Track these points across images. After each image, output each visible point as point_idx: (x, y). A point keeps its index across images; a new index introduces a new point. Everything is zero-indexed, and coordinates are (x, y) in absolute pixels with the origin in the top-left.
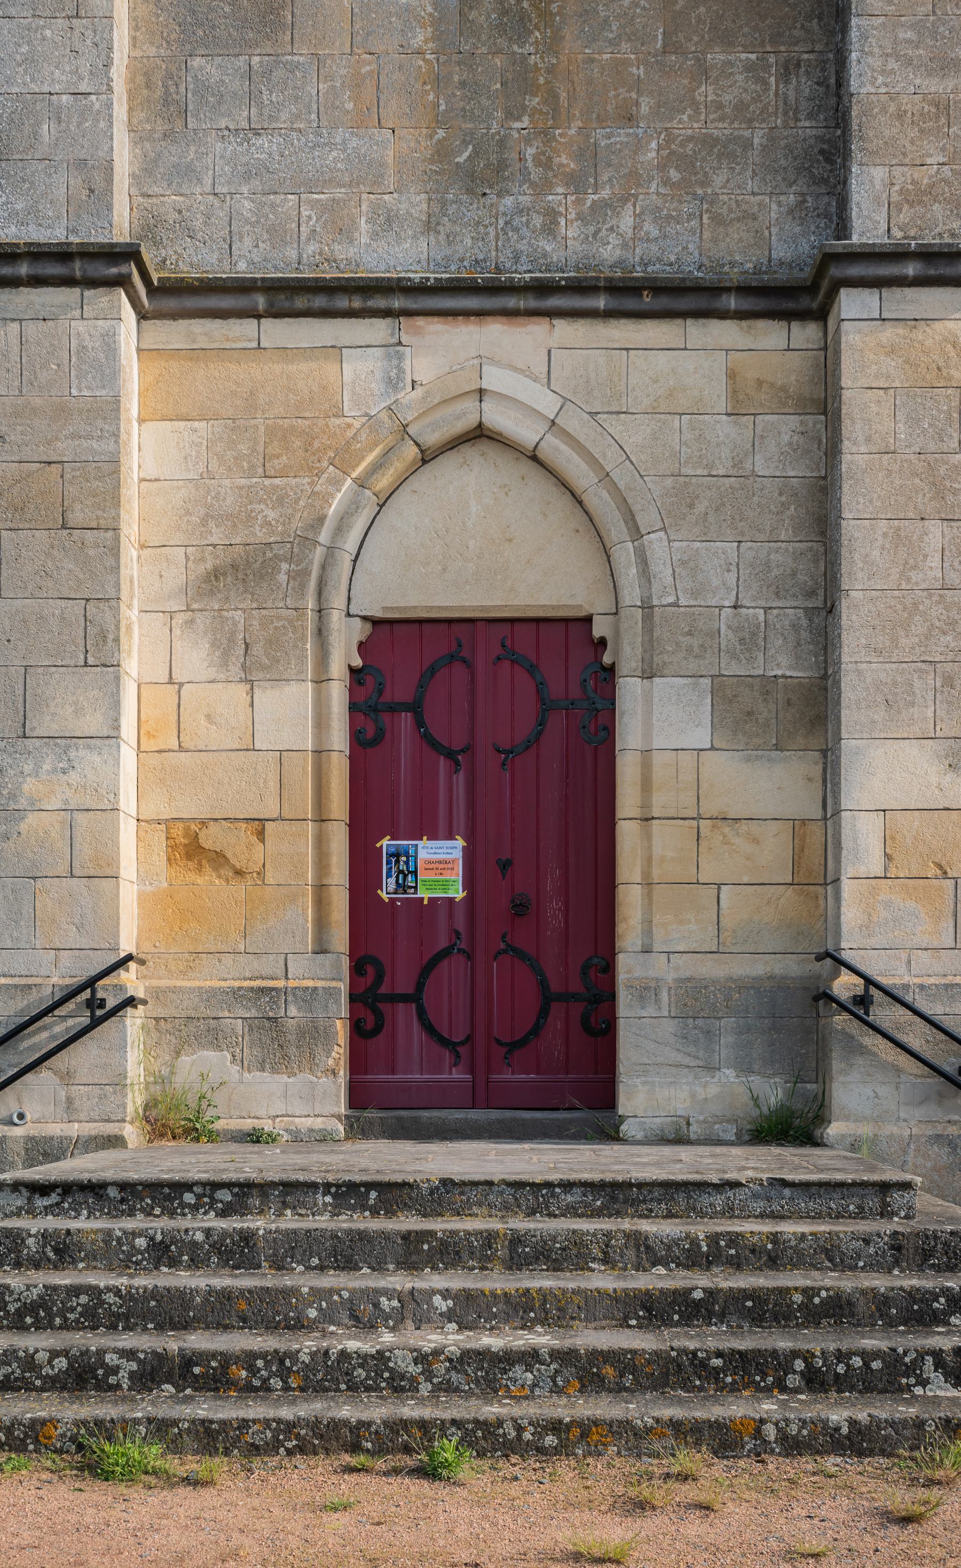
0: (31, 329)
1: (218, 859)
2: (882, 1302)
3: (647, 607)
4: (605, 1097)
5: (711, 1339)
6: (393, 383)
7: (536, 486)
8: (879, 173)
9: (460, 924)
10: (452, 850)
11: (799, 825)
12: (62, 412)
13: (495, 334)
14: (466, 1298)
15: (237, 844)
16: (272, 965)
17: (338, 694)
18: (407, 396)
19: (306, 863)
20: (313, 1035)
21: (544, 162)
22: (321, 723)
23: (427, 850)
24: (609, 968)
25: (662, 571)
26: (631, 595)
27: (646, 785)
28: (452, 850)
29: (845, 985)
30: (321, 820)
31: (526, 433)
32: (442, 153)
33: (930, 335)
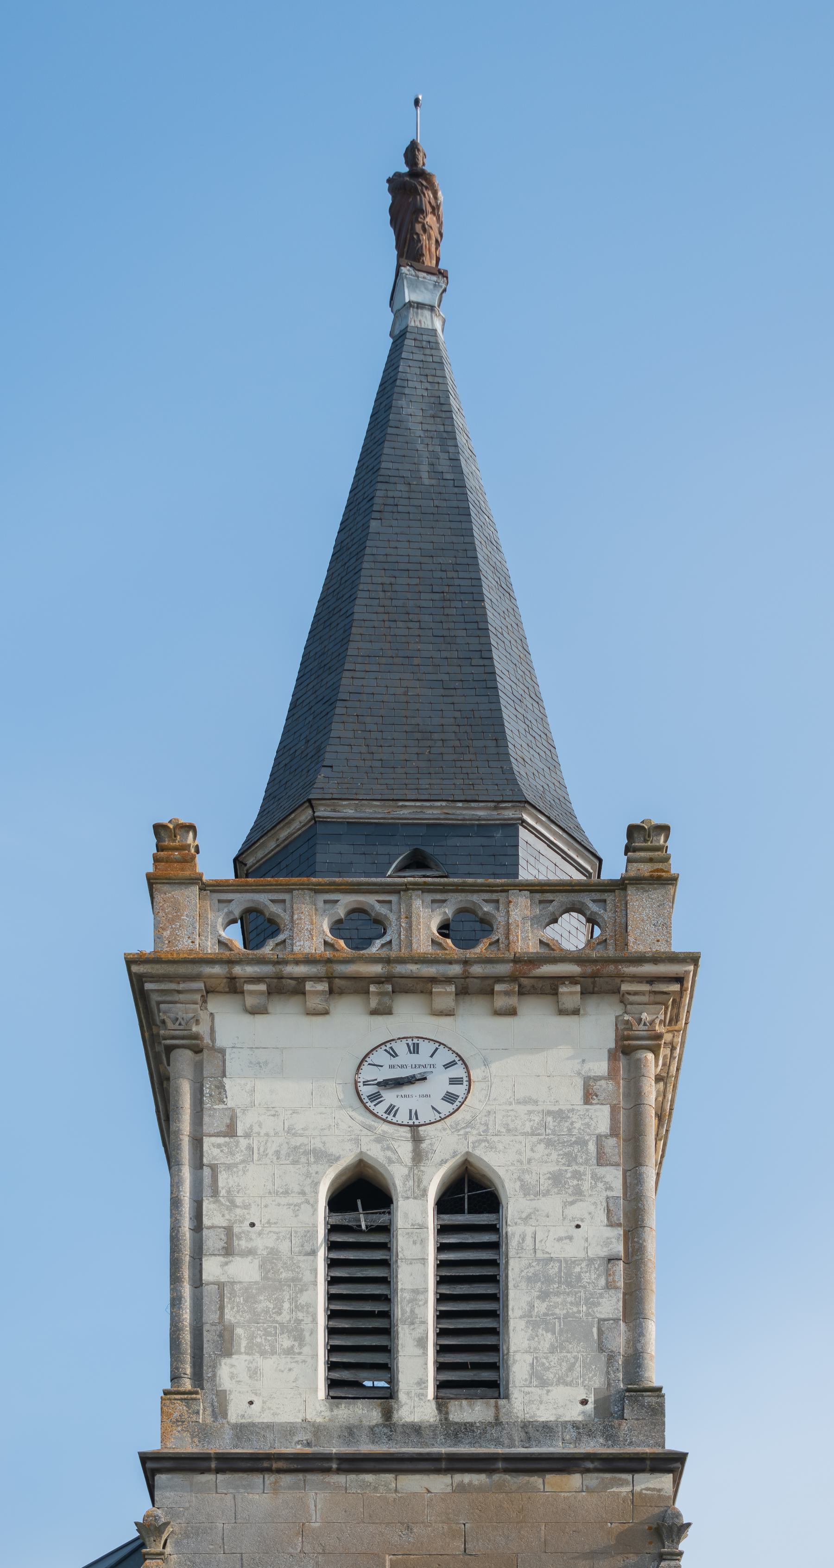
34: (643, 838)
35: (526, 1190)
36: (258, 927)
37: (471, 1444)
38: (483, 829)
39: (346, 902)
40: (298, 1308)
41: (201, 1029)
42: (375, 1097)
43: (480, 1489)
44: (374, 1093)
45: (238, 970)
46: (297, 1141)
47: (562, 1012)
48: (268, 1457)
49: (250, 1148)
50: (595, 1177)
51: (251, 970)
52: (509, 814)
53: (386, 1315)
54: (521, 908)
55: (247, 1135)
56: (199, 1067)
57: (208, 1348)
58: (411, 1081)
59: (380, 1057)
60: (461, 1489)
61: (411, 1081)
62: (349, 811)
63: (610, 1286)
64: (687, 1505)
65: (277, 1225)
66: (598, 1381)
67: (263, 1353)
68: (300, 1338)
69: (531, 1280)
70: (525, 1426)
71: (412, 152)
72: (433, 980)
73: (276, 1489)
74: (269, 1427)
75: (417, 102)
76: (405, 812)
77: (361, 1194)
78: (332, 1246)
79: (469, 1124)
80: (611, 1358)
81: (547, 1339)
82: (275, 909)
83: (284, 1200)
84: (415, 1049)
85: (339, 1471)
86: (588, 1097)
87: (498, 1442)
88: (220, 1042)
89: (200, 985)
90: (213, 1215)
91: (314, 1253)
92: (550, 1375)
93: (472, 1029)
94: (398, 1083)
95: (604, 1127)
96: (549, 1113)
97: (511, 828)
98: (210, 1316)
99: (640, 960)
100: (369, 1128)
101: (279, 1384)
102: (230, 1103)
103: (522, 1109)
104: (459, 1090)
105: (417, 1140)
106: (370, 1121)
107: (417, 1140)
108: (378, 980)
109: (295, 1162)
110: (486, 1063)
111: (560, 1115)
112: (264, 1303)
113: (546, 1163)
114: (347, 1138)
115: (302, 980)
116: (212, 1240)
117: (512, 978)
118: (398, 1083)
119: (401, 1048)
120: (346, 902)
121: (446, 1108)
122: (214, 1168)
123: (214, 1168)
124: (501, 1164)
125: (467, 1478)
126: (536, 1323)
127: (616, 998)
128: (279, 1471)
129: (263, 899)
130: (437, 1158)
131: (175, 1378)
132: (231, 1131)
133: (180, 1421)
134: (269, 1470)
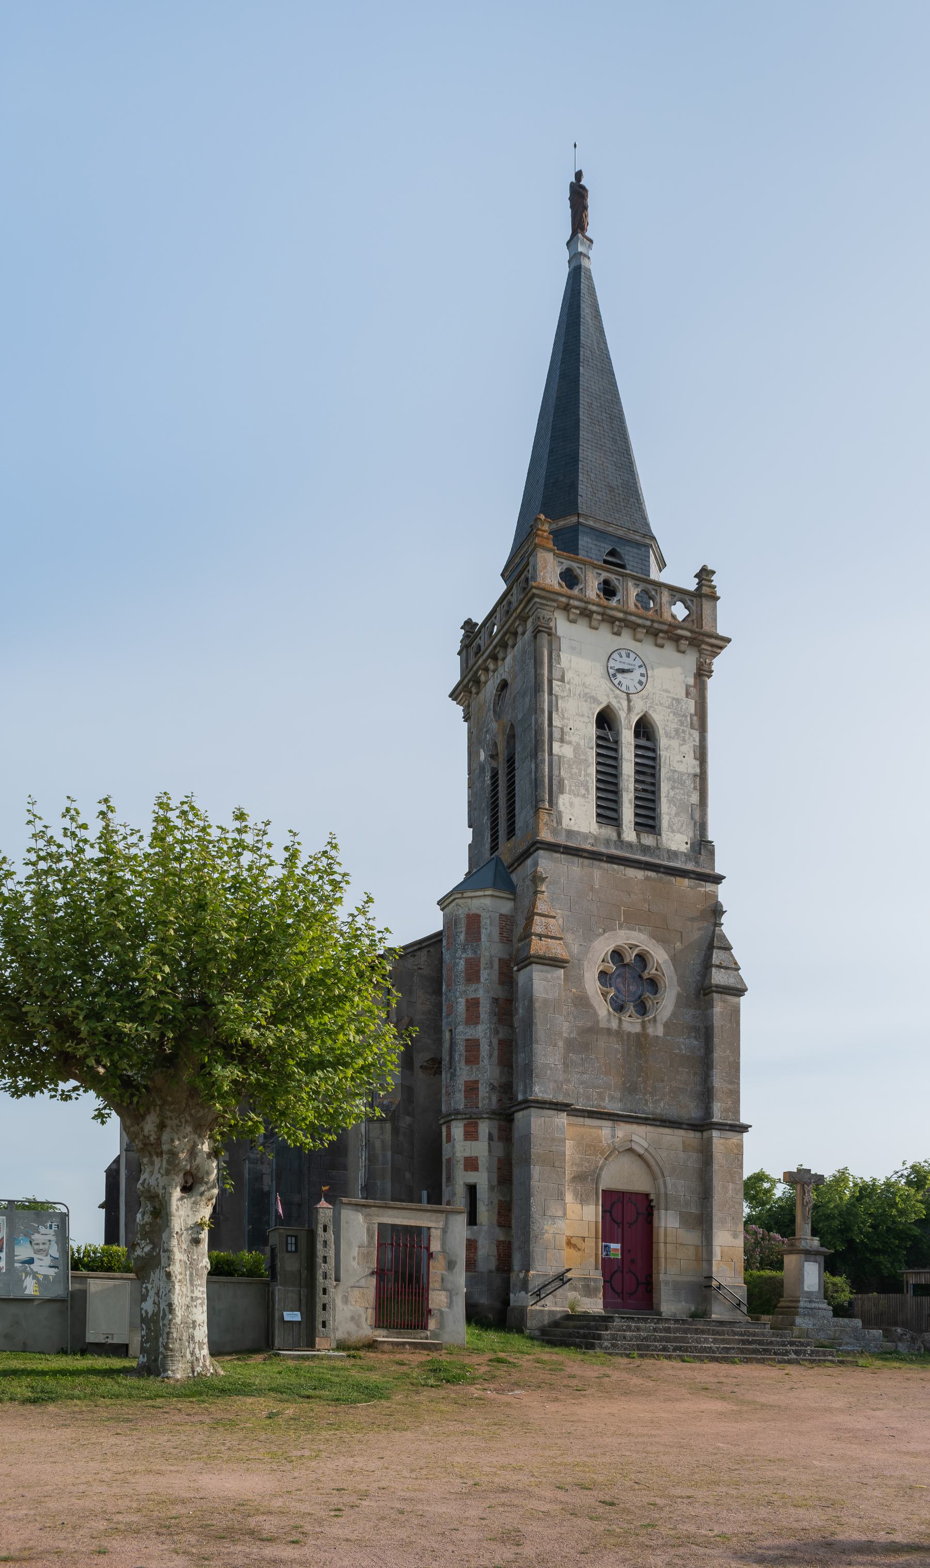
0: (547, 1119)
1: (575, 1246)
2: (778, 1342)
6: (613, 1136)
7: (640, 1162)
9: (620, 1265)
10: (618, 1246)
12: (553, 1140)
13: (634, 1127)
14: (714, 1339)
18: (617, 1140)
20: (596, 1289)
21: (645, 1089)
22: (597, 1215)
25: (669, 1186)
26: (662, 1191)
27: (666, 1235)
28: (618, 1246)
30: (597, 1238)
31: (641, 1151)
32: (624, 1083)
34: (704, 575)
35: (668, 736)
37: (650, 857)
41: (552, 624)
42: (614, 675)
43: (654, 880)
44: (615, 674)
45: (572, 602)
46: (587, 691)
49: (570, 690)
50: (691, 735)
51: (576, 603)
55: (569, 683)
59: (615, 656)
63: (695, 788)
66: (691, 834)
67: (574, 795)
69: (669, 779)
70: (669, 851)
71: (579, 175)
72: (639, 625)
74: (578, 833)
75: (575, 146)
80: (695, 823)
82: (579, 571)
83: (582, 719)
85: (607, 862)
86: (688, 694)
87: (659, 858)
89: (555, 604)
90: (556, 722)
94: (623, 671)
95: (692, 711)
96: (674, 699)
98: (555, 772)
100: (612, 690)
102: (562, 666)
103: (665, 694)
104: (644, 679)
105: (629, 700)
106: (613, 687)
107: (629, 700)
108: (620, 620)
109: (586, 701)
110: (653, 669)
111: (678, 701)
112: (575, 770)
115: (592, 612)
116: (556, 734)
117: (666, 632)
118: (623, 671)
119: (623, 653)
121: (639, 687)
123: (557, 696)
125: (650, 873)
126: (671, 801)
127: (696, 649)
128: (585, 857)
132: (562, 680)
134: (581, 856)
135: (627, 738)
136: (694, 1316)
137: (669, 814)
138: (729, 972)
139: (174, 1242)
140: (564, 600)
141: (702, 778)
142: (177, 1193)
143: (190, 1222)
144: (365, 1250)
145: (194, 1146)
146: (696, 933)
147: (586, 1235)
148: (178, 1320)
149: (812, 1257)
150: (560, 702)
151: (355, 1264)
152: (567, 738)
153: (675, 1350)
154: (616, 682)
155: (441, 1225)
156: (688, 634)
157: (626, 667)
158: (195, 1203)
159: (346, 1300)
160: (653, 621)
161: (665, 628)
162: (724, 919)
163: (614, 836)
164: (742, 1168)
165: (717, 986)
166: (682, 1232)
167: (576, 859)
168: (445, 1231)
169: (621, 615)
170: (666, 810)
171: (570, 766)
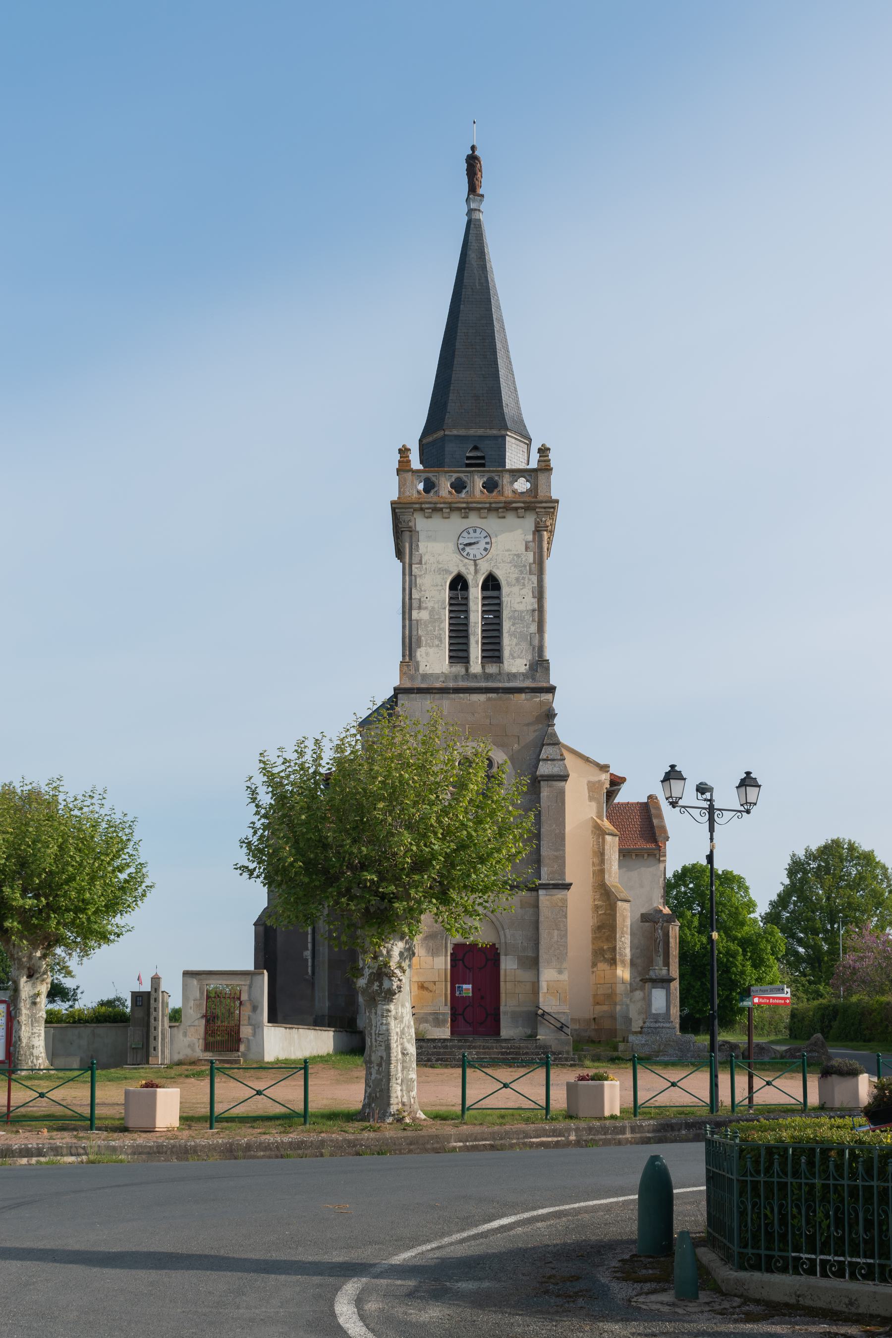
1: (427, 989)
3: (506, 943)
4: (498, 1033)
5: (407, 640)
8: (546, 869)
10: (470, 986)
11: (533, 983)
15: (431, 986)
16: (437, 1008)
17: (449, 958)
19: (443, 989)
20: (444, 1022)
23: (465, 986)
24: (499, 1009)
26: (503, 941)
27: (506, 976)
28: (470, 986)
29: (540, 1012)
30: (446, 981)
33: (555, 898)
35: (509, 584)
36: (429, 486)
38: (496, 438)
39: (455, 475)
40: (440, 629)
42: (463, 549)
43: (495, 699)
44: (463, 549)
46: (440, 566)
47: (519, 517)
48: (432, 689)
50: (529, 579)
51: (427, 506)
52: (503, 432)
53: (467, 631)
54: (507, 478)
56: (411, 537)
57: (413, 645)
58: (474, 543)
59: (465, 534)
60: (489, 699)
61: (474, 543)
62: (455, 432)
63: (533, 621)
64: (557, 706)
65: (436, 595)
66: (530, 657)
68: (441, 641)
69: (510, 618)
71: (473, 148)
72: (481, 508)
73: (434, 699)
74: (431, 675)
76: (472, 432)
77: (459, 584)
78: (450, 605)
79: (491, 559)
80: (534, 648)
81: (515, 641)
84: (475, 531)
86: (527, 549)
87: (500, 681)
88: (418, 529)
91: (445, 608)
92: (515, 655)
93: (492, 523)
95: (531, 561)
97: (503, 437)
98: (414, 633)
99: (541, 502)
101: (435, 660)
103: (507, 553)
104: (488, 546)
105: (476, 565)
107: (476, 565)
108: (464, 508)
111: (518, 556)
113: (514, 574)
114: (455, 564)
116: (415, 604)
119: (471, 531)
120: (455, 475)
121: (484, 553)
122: (415, 576)
123: (415, 576)
124: (500, 574)
125: (491, 695)
129: (430, 475)
130: (482, 572)
131: (404, 656)
132: (420, 563)
133: (405, 673)
135: (476, 594)
136: (530, 1036)
137: (510, 645)
138: (555, 762)
139: (22, 1004)
140: (417, 506)
141: (540, 610)
142: (24, 979)
143: (31, 994)
144: (198, 1002)
145: (31, 954)
146: (531, 735)
147: (437, 979)
148: (24, 1045)
149: (660, 984)
150: (418, 579)
151: (191, 1011)
152: (424, 605)
153: (437, 1060)
154: (465, 554)
155: (248, 983)
156: (522, 505)
157: (472, 541)
158: (34, 983)
159: (185, 1034)
160: (490, 503)
161: (501, 505)
162: (556, 721)
163: (463, 671)
164: (566, 918)
165: (542, 776)
166: (520, 972)
167: (428, 696)
168: (250, 987)
169: (464, 505)
170: (508, 643)
171: (426, 626)
